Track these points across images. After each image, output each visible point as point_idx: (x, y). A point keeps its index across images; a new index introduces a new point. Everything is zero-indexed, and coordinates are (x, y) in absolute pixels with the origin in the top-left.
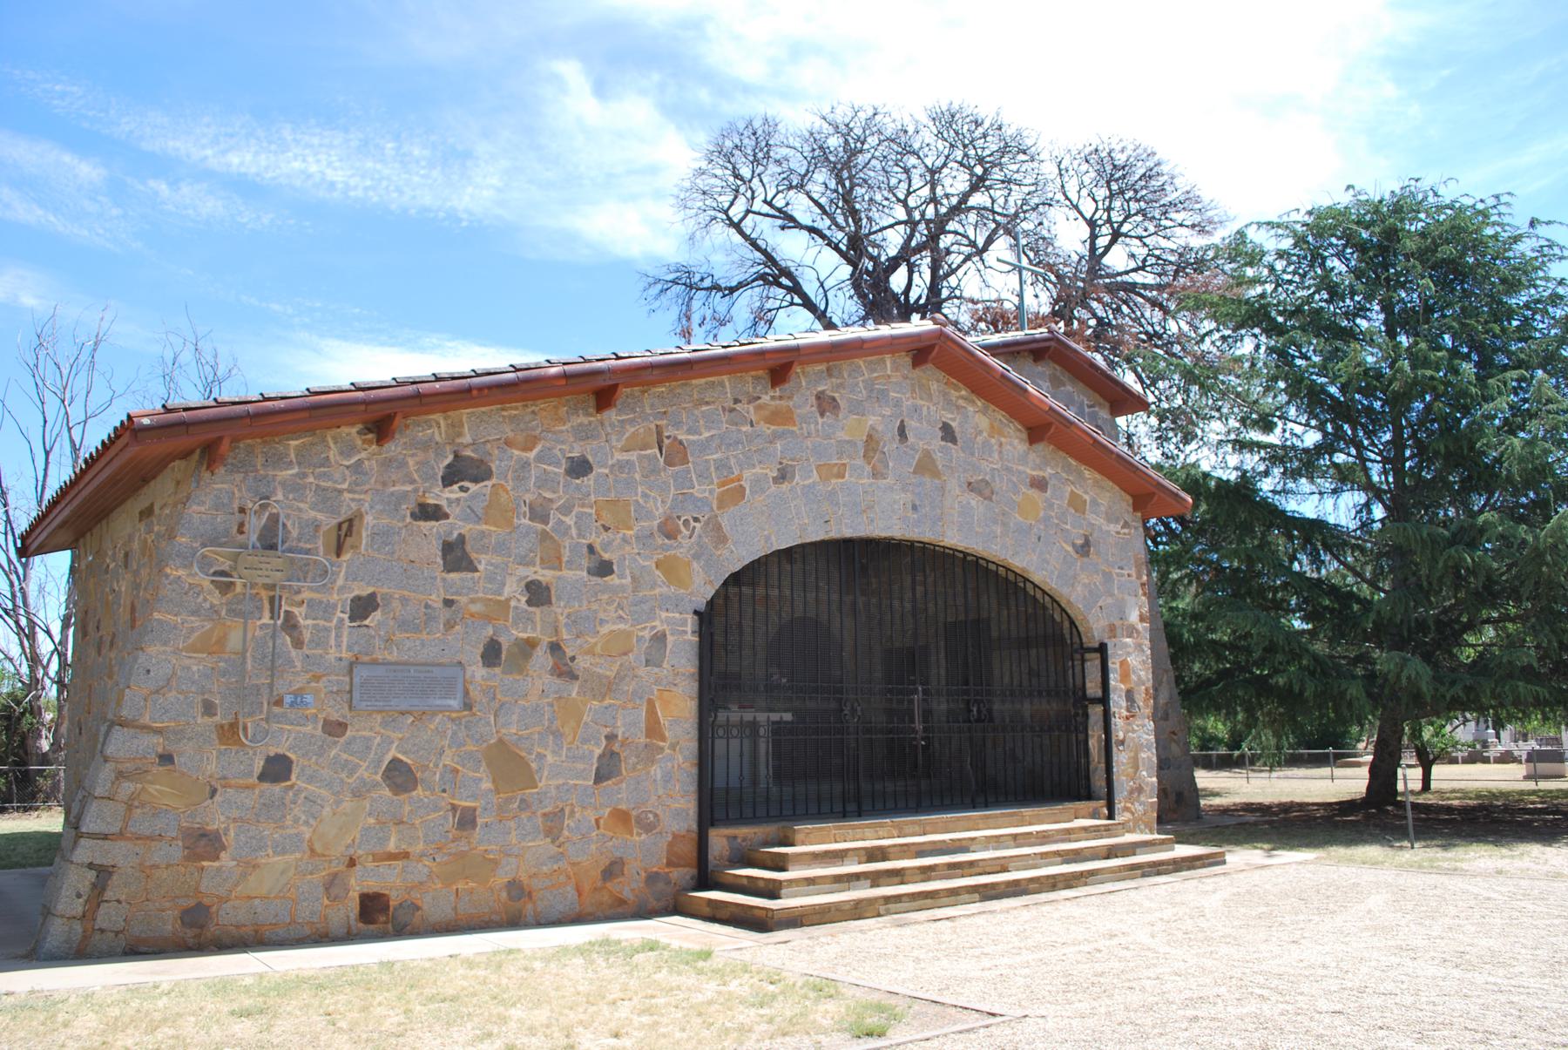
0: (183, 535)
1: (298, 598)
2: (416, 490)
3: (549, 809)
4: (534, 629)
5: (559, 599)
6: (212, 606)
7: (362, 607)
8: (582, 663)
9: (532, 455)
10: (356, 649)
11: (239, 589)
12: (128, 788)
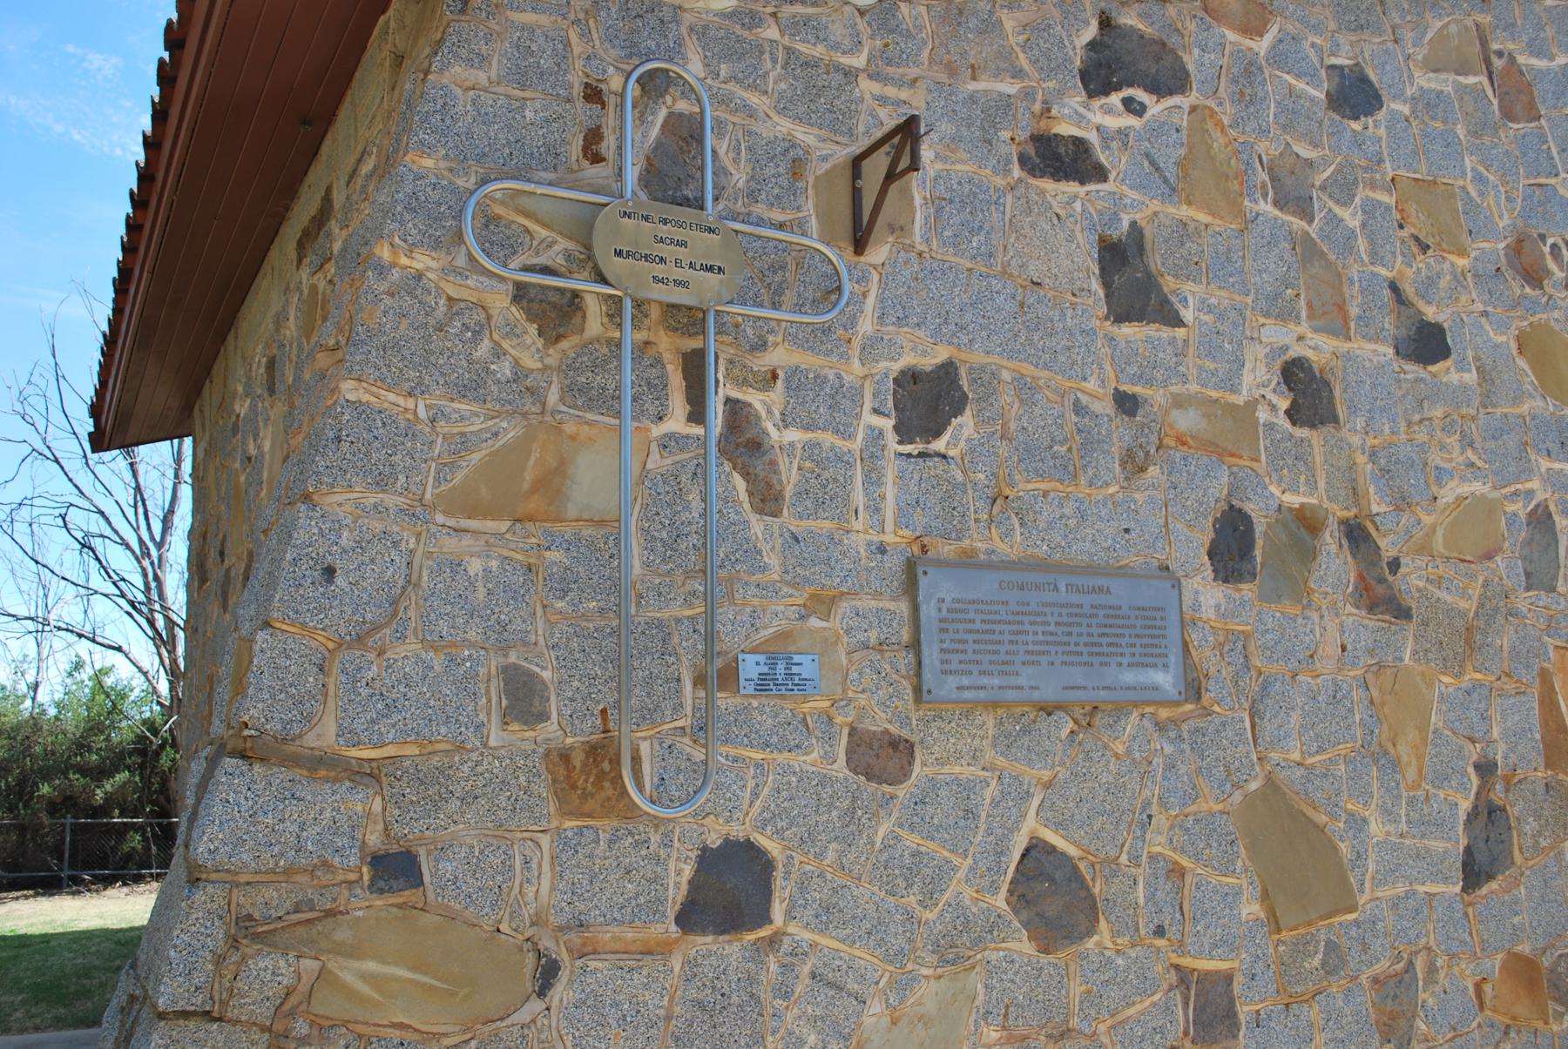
0: (426, 149)
1: (763, 362)
2: (1028, 95)
3: (1380, 967)
4: (1312, 485)
5: (1353, 410)
6: (519, 374)
7: (927, 401)
8: (1412, 580)
9: (1262, 45)
10: (920, 519)
11: (594, 321)
12: (269, 971)
